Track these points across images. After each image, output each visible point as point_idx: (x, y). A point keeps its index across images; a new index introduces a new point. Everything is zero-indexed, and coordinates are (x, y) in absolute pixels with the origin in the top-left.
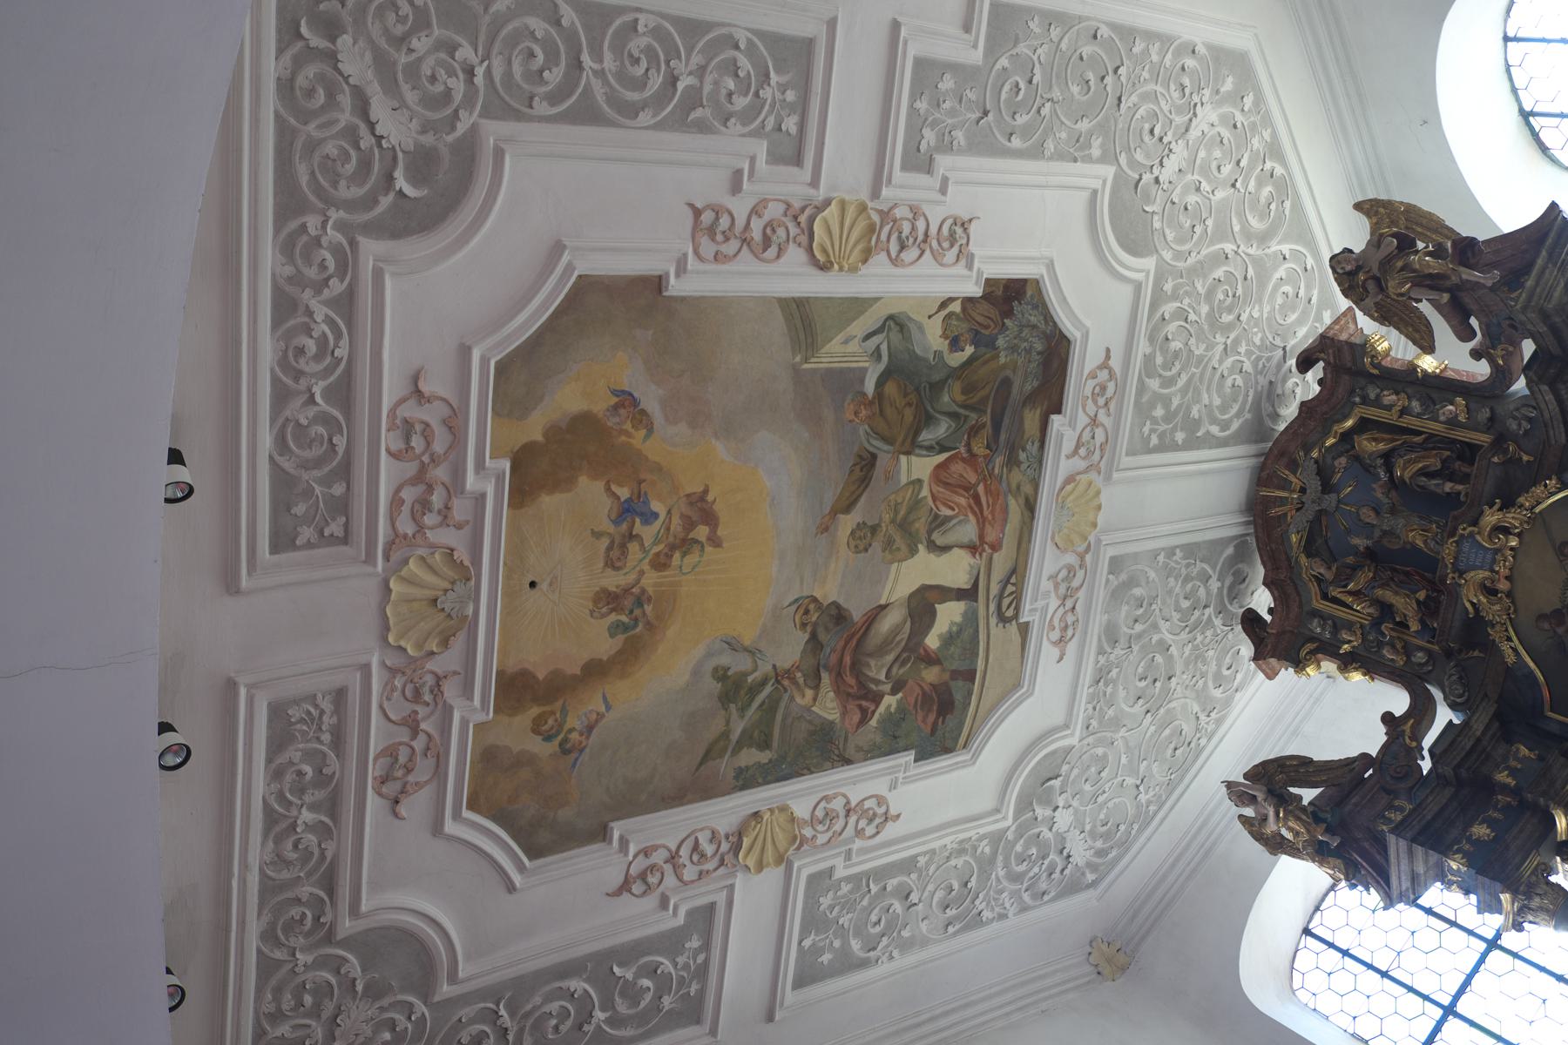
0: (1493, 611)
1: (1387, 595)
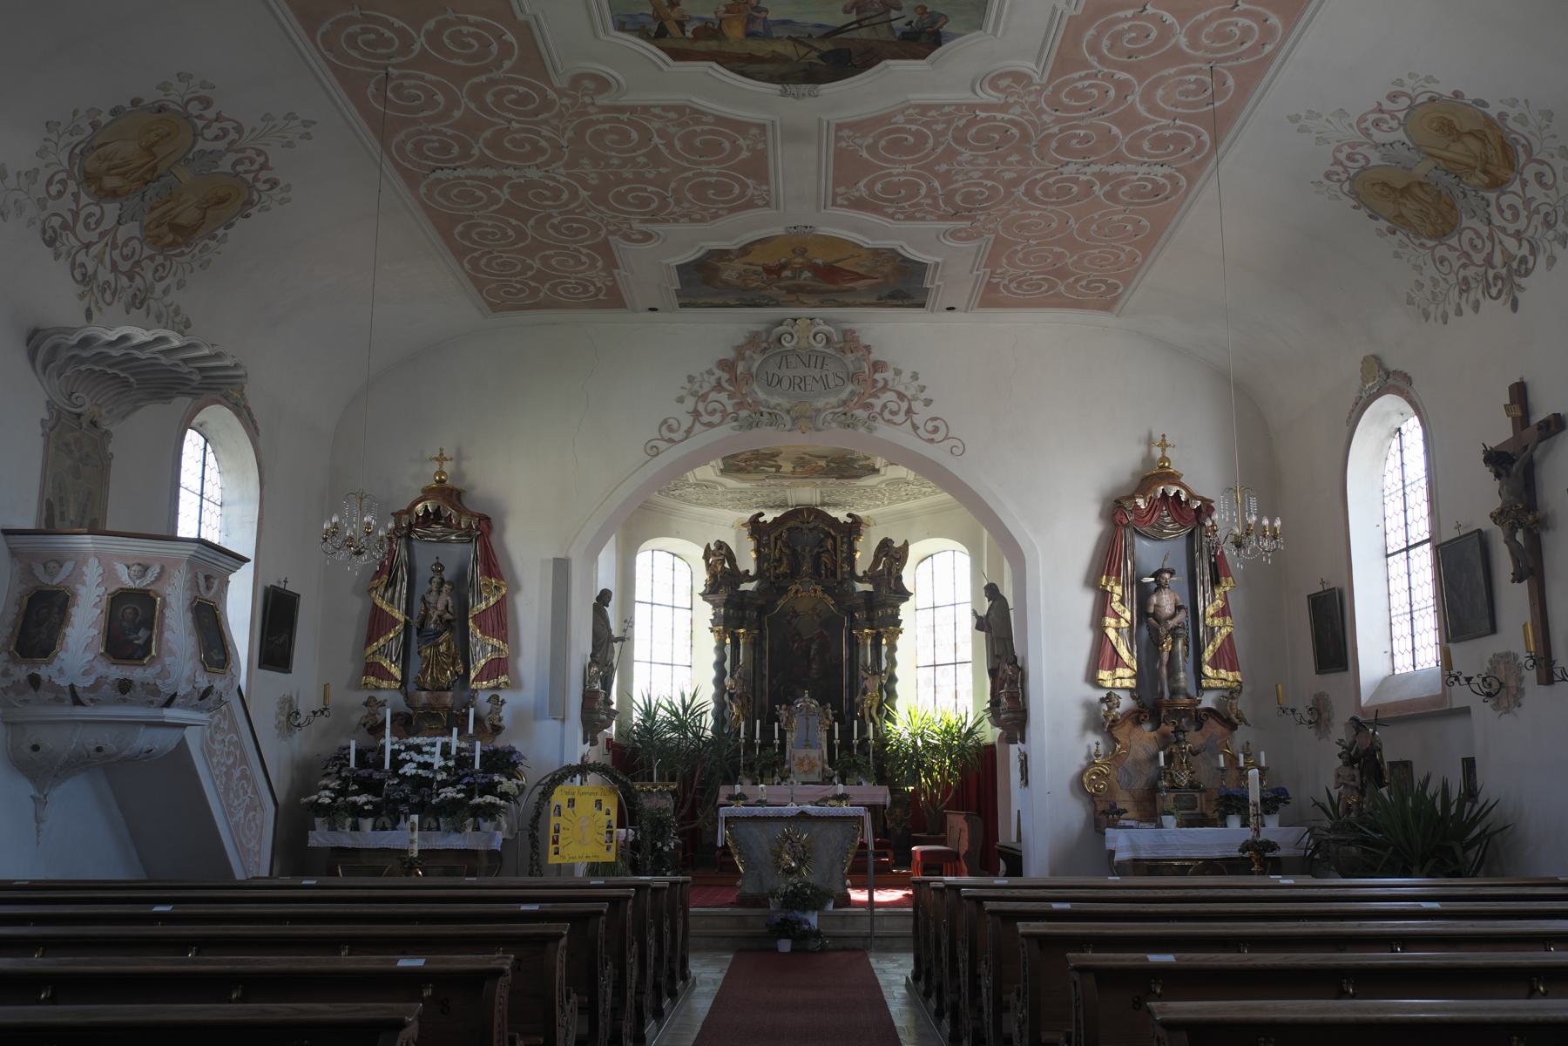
0: (791, 594)
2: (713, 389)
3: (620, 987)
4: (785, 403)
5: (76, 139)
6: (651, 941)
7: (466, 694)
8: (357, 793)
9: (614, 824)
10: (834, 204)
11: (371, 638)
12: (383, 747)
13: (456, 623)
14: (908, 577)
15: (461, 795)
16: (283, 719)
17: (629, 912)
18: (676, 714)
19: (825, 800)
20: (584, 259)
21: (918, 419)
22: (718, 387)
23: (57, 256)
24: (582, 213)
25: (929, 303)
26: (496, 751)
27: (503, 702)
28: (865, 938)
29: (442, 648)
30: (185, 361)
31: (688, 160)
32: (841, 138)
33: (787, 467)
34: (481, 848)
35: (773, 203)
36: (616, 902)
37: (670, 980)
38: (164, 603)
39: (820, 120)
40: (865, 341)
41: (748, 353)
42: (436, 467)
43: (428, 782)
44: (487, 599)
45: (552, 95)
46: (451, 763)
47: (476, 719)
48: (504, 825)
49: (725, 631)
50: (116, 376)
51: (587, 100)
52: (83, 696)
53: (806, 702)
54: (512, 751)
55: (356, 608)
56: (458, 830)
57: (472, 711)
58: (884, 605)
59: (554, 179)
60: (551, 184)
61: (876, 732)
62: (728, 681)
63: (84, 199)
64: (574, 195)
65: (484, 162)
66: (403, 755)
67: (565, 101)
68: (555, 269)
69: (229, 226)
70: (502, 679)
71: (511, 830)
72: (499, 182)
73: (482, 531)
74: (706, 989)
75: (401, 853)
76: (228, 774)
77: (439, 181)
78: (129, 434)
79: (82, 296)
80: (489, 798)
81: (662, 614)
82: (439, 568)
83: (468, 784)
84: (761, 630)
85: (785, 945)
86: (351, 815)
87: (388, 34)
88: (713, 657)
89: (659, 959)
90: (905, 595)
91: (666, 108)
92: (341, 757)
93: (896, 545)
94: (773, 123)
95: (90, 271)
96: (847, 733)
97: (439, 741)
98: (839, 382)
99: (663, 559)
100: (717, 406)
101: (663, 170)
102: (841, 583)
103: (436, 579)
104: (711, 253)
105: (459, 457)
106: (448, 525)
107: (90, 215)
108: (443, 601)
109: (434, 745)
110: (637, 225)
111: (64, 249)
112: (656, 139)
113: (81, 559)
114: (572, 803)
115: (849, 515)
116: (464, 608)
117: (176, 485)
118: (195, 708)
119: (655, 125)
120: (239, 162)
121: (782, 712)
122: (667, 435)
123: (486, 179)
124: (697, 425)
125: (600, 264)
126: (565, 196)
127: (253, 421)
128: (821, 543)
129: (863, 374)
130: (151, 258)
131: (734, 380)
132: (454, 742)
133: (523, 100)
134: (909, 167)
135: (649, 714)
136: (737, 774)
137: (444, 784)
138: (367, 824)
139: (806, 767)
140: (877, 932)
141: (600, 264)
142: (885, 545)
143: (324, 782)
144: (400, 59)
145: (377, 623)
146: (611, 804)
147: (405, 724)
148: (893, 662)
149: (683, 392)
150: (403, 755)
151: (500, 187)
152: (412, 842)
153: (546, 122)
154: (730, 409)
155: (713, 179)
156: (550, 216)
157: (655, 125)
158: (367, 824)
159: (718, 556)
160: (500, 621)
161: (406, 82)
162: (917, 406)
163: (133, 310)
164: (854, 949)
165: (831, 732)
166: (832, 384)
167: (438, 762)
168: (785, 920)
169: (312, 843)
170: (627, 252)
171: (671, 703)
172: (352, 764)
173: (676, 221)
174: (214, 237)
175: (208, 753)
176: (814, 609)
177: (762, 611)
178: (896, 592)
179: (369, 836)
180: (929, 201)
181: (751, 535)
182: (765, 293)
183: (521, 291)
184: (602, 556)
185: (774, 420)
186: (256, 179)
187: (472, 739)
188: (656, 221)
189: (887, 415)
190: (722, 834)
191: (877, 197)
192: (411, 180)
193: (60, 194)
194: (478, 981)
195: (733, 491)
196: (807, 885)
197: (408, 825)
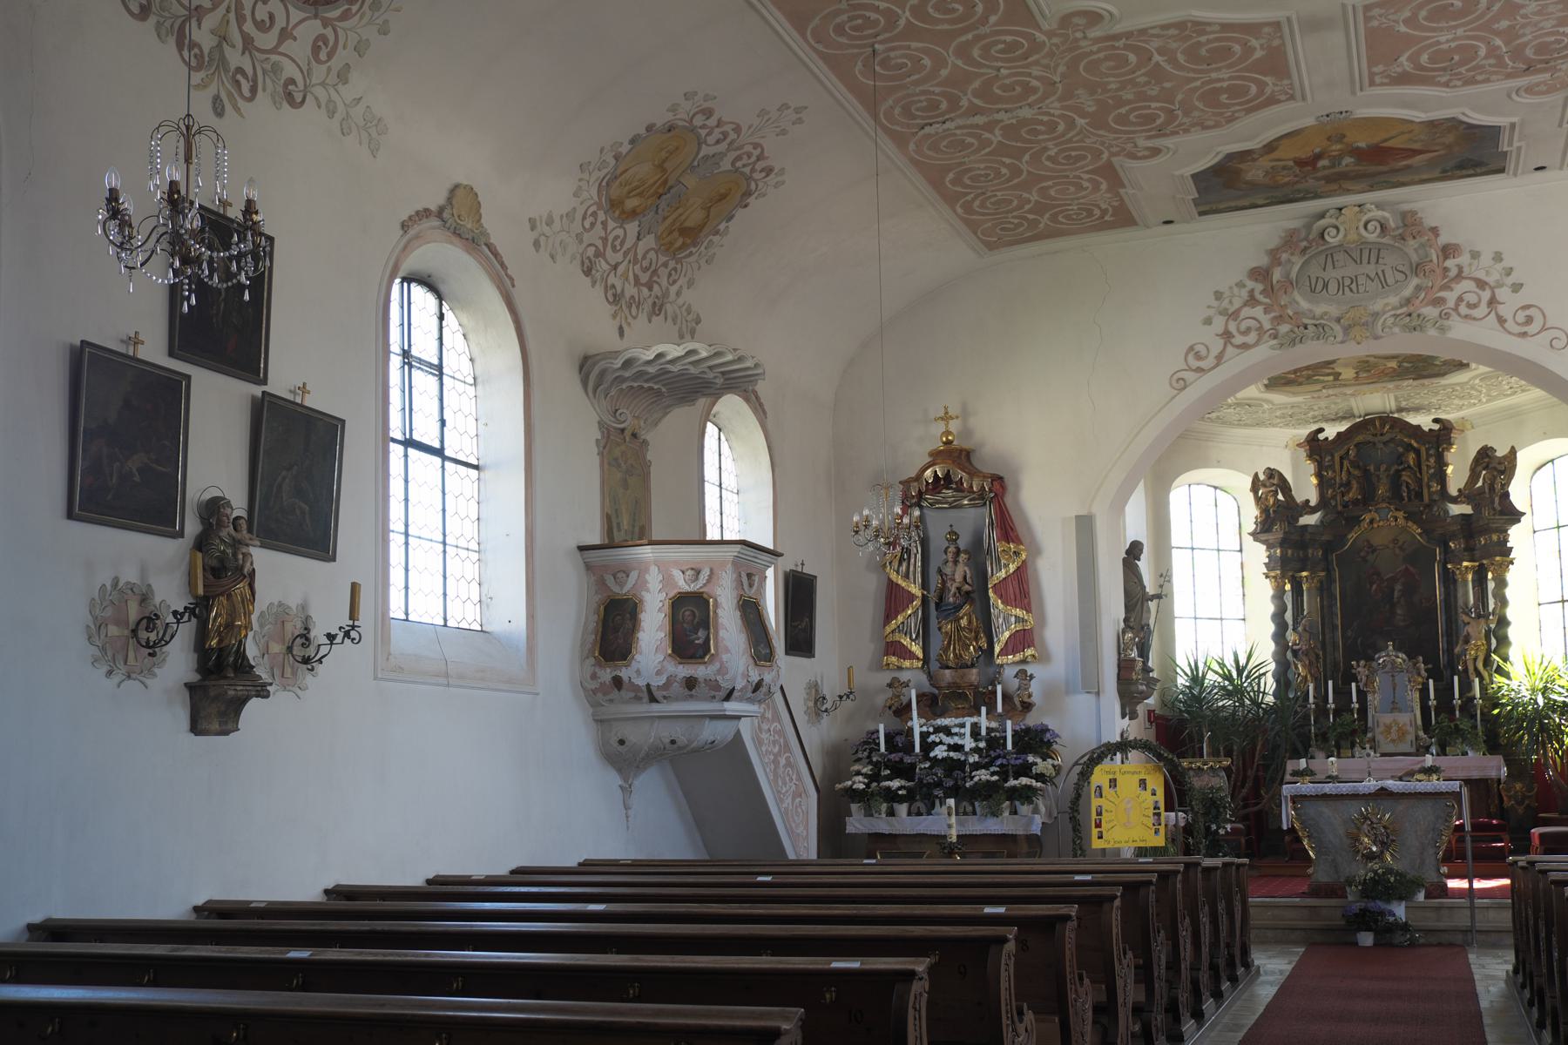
0: (1365, 525)
1: (1355, 485)
2: (1245, 304)
3: (1174, 965)
4: (1334, 311)
5: (605, 171)
6: (1205, 920)
7: (991, 670)
8: (889, 778)
9: (1162, 805)
10: (1372, 83)
11: (889, 616)
12: (911, 730)
13: (976, 594)
14: (1517, 493)
15: (995, 778)
16: (811, 704)
17: (1179, 886)
18: (1228, 677)
19: (1411, 774)
20: (1085, 184)
21: (1503, 310)
22: (1252, 301)
23: (594, 283)
24: (1082, 141)
25: (1511, 166)
26: (1028, 730)
27: (1032, 677)
28: (1465, 932)
29: (964, 622)
30: (710, 368)
31: (1194, 71)
32: (1373, 18)
33: (1348, 374)
34: (1021, 832)
35: (1298, 94)
36: (1164, 876)
37: (1232, 966)
38: (716, 604)
39: (1344, 6)
40: (1430, 222)
41: (1284, 256)
42: (941, 427)
43: (960, 765)
44: (1006, 566)
45: (1040, 37)
46: (982, 745)
47: (1005, 696)
48: (1042, 809)
49: (1283, 576)
50: (651, 389)
51: (1079, 35)
52: (657, 694)
53: (1391, 655)
54: (1045, 730)
55: (871, 585)
56: (995, 814)
57: (999, 688)
58: (1487, 530)
59: (1048, 114)
60: (1045, 118)
61: (1483, 688)
62: (1291, 637)
63: (611, 224)
64: (1071, 124)
65: (974, 111)
66: (932, 738)
67: (1055, 40)
68: (1055, 199)
69: (730, 218)
70: (1029, 652)
71: (1049, 814)
72: (989, 127)
73: (995, 491)
74: (1271, 978)
75: (940, 839)
76: (776, 762)
77: (929, 136)
78: (662, 436)
79: (614, 316)
80: (1024, 781)
81: (1206, 560)
82: (953, 536)
83: (1001, 766)
84: (1328, 570)
85: (1366, 939)
86: (886, 801)
87: (874, 16)
88: (1270, 608)
89: (1215, 944)
90: (1515, 516)
91: (1165, 27)
92: (870, 742)
93: (1499, 454)
94: (1289, 19)
95: (619, 290)
96: (1445, 692)
97: (969, 721)
98: (1400, 277)
99: (1203, 494)
100: (1252, 323)
101: (1167, 85)
102: (1428, 506)
103: (952, 549)
104: (1230, 157)
105: (965, 413)
106: (959, 489)
107: (616, 238)
108: (961, 572)
109: (962, 726)
110: (1142, 143)
111: (598, 275)
112: (1157, 58)
113: (643, 568)
114: (1113, 783)
115: (1436, 421)
116: (982, 577)
117: (702, 481)
118: (750, 701)
119: (1154, 45)
120: (739, 158)
121: (1361, 670)
122: (1195, 364)
123: (977, 126)
124: (1230, 349)
125: (1104, 186)
126: (1061, 127)
127: (761, 405)
128: (1400, 459)
129: (1428, 259)
130: (665, 265)
131: (1270, 290)
132: (984, 722)
133: (1012, 47)
134: (1460, 32)
135: (1197, 680)
136: (1307, 747)
137: (976, 766)
138: (902, 809)
139: (1394, 735)
140: (1478, 926)
141: (1104, 186)
142: (1485, 454)
143: (856, 767)
144: (887, 35)
145: (894, 599)
146: (1156, 783)
147: (932, 704)
148: (1503, 602)
149: (1211, 312)
150: (932, 738)
151: (991, 132)
152: (950, 826)
153: (1037, 63)
154: (1267, 326)
155: (1225, 84)
156: (1046, 149)
157: (1154, 45)
158: (902, 809)
159: (1270, 486)
160: (1021, 590)
161: (892, 54)
162: (1503, 294)
163: (655, 318)
164: (1451, 945)
165: (1424, 692)
166: (1390, 281)
167: (969, 743)
168: (1364, 911)
169: (850, 829)
170: (1131, 169)
171: (1222, 665)
172: (883, 749)
173: (1186, 131)
174: (717, 233)
175: (758, 742)
176: (1395, 541)
177: (1328, 548)
178: (1502, 513)
179: (904, 822)
180: (1492, 61)
181: (1310, 457)
182: (1299, 186)
183: (1020, 225)
184: (1128, 509)
185: (1321, 331)
186: (753, 170)
187: (1001, 718)
188: (1165, 135)
189: (1463, 310)
190: (1287, 816)
191: (1423, 68)
192: (900, 140)
193: (593, 225)
194: (1050, 925)
195: (1284, 406)
196: (1390, 871)
197: (944, 809)
